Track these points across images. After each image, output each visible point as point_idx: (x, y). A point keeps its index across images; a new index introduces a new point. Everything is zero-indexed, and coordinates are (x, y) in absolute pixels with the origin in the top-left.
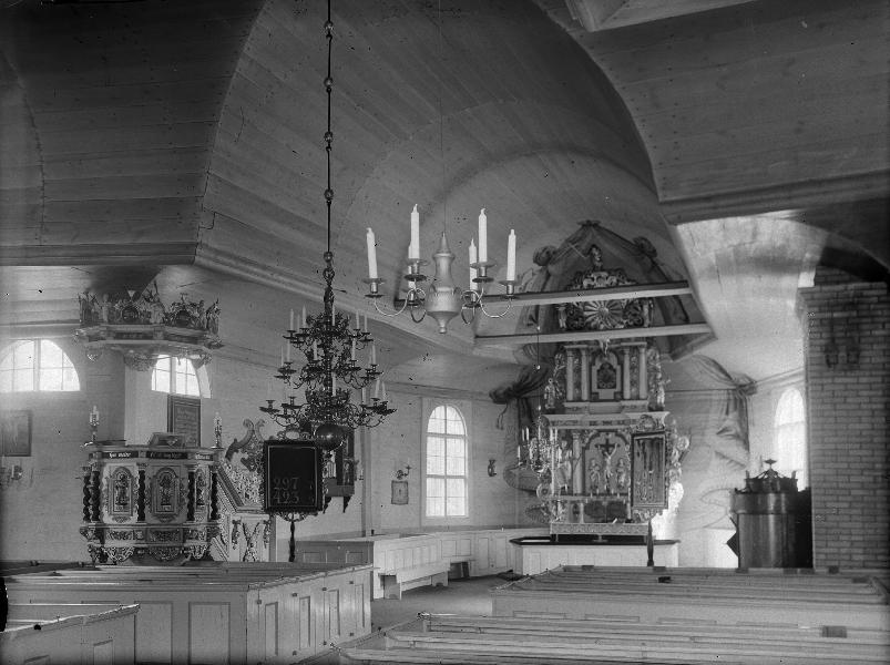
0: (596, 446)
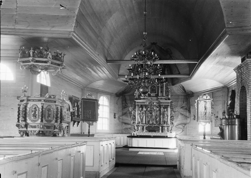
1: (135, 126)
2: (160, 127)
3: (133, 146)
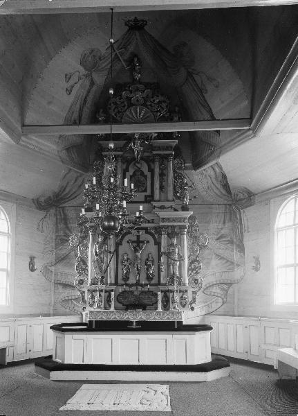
0: (128, 242)
2: (160, 295)
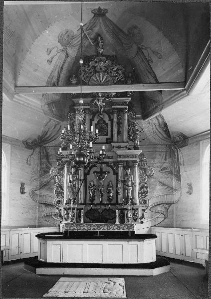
0: (94, 173)
1: (63, 209)
3: (48, 261)
